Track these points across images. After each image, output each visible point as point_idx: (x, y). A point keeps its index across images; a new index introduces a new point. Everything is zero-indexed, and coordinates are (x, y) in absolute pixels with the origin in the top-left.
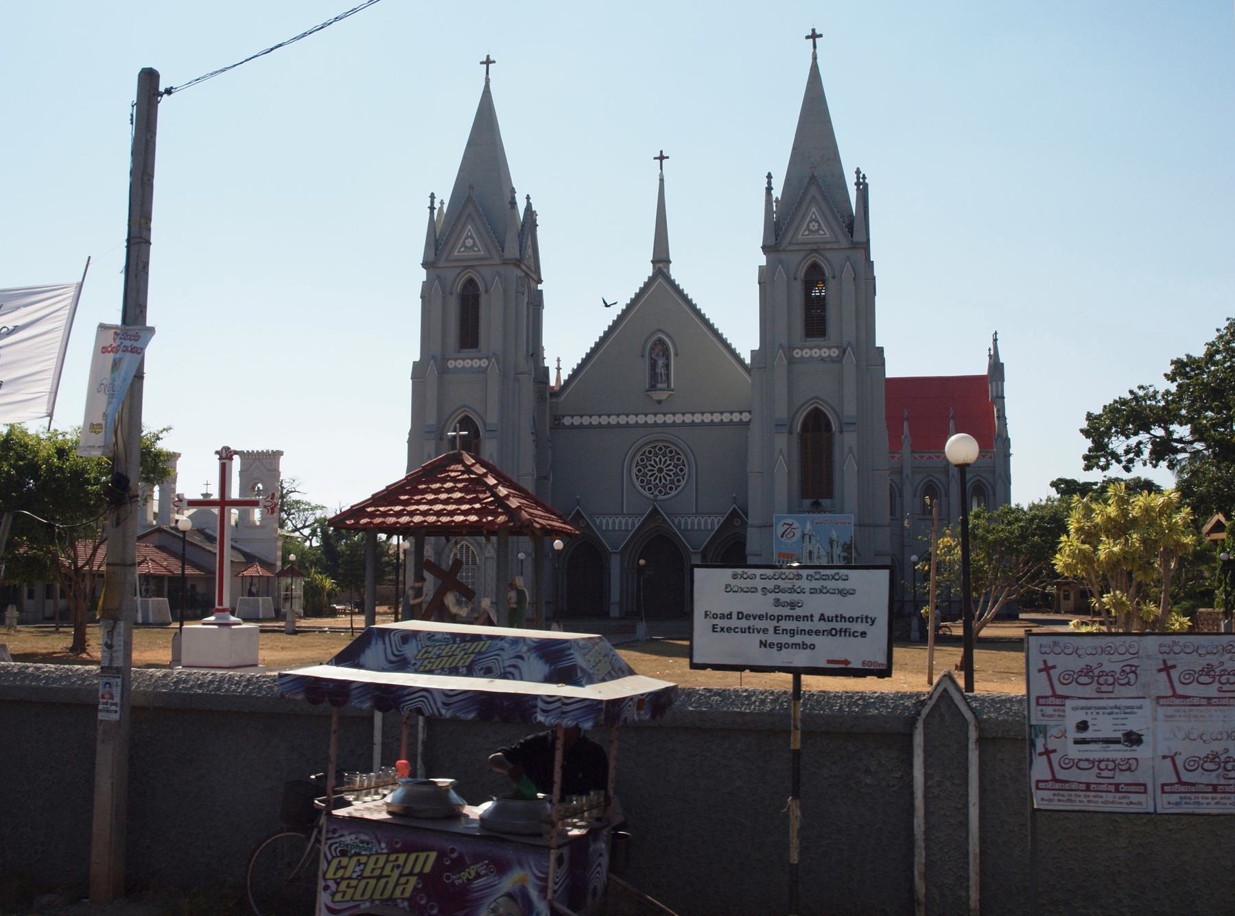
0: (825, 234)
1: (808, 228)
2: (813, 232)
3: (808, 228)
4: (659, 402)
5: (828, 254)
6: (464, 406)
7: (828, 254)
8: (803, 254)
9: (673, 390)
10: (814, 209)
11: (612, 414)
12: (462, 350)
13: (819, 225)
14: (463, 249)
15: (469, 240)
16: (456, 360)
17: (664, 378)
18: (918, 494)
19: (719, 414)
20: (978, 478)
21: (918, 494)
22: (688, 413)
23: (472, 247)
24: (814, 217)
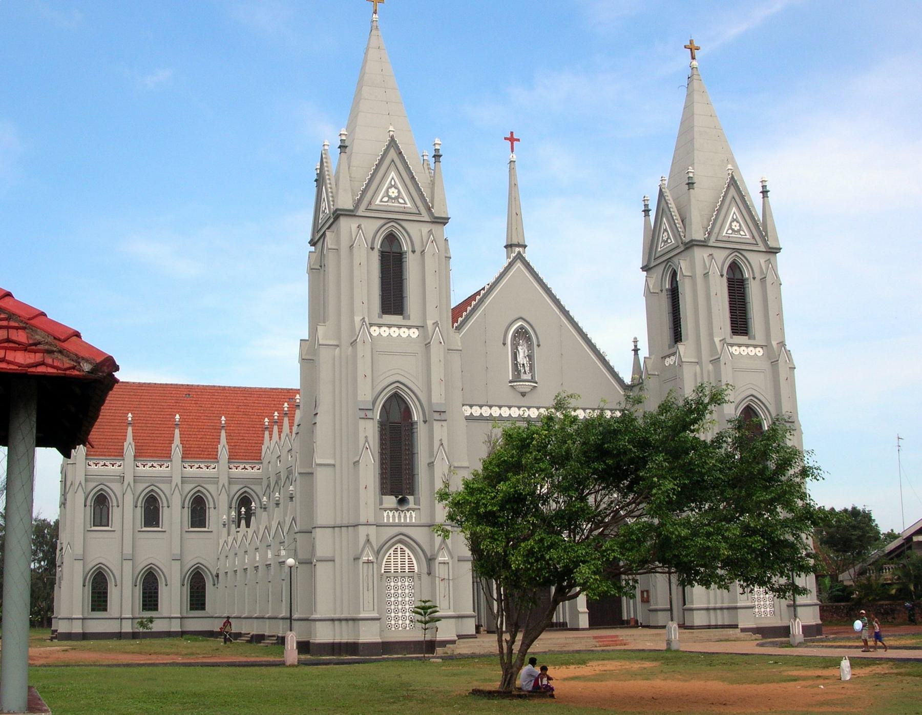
0: (746, 235)
1: (730, 228)
2: (735, 231)
3: (730, 228)
4: (523, 394)
5: (749, 255)
6: (398, 382)
7: (749, 255)
8: (380, 222)
9: (536, 383)
10: (393, 174)
11: (578, 408)
12: (384, 316)
13: (399, 192)
14: (386, 199)
15: (393, 189)
16: (380, 326)
17: (527, 369)
18: (233, 505)
19: (516, 409)
20: (152, 487)
21: (233, 505)
22: (496, 406)
23: (397, 198)
24: (393, 183)
